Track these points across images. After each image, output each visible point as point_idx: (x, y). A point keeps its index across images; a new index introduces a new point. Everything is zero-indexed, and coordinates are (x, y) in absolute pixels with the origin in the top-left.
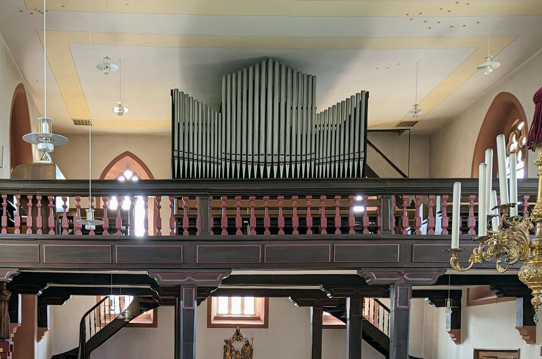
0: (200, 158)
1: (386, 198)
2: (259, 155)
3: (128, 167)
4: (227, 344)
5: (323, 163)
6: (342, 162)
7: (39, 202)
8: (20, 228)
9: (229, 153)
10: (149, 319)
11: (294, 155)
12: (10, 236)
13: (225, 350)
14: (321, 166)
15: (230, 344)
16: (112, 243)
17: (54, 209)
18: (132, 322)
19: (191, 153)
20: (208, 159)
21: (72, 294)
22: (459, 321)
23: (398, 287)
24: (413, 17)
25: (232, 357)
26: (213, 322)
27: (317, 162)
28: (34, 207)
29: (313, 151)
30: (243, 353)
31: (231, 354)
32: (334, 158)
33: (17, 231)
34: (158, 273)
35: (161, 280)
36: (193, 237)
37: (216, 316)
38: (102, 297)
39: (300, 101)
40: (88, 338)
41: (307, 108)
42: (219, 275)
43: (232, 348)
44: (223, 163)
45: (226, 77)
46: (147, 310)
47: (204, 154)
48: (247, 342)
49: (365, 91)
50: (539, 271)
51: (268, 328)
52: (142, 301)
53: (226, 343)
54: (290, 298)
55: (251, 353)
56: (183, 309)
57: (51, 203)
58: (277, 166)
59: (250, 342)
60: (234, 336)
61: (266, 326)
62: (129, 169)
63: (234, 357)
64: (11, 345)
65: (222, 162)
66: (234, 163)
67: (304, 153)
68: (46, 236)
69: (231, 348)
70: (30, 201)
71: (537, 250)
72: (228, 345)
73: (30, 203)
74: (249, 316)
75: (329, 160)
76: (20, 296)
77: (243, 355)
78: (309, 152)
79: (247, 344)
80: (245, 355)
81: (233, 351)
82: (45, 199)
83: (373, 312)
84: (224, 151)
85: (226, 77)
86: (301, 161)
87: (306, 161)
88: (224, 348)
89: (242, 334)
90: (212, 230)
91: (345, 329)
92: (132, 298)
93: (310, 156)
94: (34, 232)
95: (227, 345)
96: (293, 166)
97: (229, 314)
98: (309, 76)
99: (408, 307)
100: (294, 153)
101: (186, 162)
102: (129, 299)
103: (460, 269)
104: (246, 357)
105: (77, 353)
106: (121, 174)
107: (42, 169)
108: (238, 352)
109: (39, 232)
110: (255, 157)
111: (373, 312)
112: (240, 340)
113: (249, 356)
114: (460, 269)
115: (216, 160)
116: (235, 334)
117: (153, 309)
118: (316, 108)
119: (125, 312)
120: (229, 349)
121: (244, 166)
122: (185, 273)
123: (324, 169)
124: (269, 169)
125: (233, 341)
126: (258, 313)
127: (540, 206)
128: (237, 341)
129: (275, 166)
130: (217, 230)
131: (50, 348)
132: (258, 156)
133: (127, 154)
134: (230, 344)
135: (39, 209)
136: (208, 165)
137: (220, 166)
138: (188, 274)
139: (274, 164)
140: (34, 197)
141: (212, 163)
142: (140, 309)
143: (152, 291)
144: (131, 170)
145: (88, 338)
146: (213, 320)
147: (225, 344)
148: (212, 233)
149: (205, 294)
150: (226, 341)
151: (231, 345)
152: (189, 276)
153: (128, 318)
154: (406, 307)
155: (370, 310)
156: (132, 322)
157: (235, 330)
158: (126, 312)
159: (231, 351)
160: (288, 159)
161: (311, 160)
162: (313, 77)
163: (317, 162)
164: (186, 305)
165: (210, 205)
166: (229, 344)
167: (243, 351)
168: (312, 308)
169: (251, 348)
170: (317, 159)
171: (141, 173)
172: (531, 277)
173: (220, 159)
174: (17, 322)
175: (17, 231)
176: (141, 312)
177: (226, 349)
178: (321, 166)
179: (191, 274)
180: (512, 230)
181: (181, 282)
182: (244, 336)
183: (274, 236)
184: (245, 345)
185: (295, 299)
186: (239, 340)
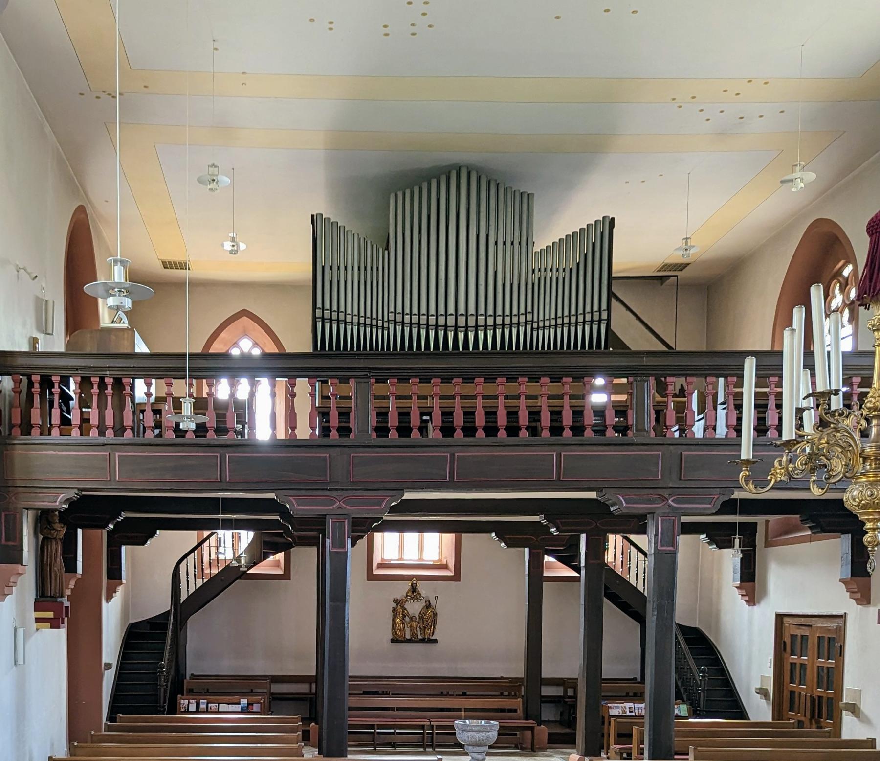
0: (355, 319)
1: (640, 381)
3: (245, 334)
4: (397, 605)
5: (544, 327)
7: (110, 387)
8: (80, 428)
9: (401, 312)
11: (499, 316)
12: (65, 439)
13: (394, 615)
14: (541, 332)
16: (222, 450)
17: (133, 398)
19: (342, 312)
20: (368, 321)
21: (160, 529)
23: (660, 518)
26: (376, 572)
27: (535, 325)
28: (102, 396)
29: (529, 309)
31: (403, 621)
32: (561, 319)
33: (75, 432)
36: (344, 441)
37: (380, 562)
38: (206, 534)
40: (184, 597)
41: (520, 243)
42: (385, 499)
44: (392, 327)
45: (396, 196)
49: (609, 217)
52: (267, 539)
53: (395, 604)
54: (493, 535)
55: (435, 619)
57: (128, 388)
58: (473, 332)
59: (433, 603)
60: (408, 592)
61: (456, 577)
62: (247, 337)
63: (407, 625)
64: (67, 608)
65: (390, 325)
67: (515, 312)
68: (120, 440)
69: (403, 612)
70: (95, 386)
72: (399, 607)
73: (95, 389)
74: (432, 563)
75: (553, 322)
76: (80, 531)
77: (422, 622)
78: (522, 311)
79: (428, 606)
80: (425, 622)
81: (407, 617)
82: (118, 384)
84: (392, 309)
85: (396, 196)
86: (511, 325)
87: (519, 324)
88: (392, 611)
89: (420, 590)
90: (374, 430)
92: (251, 534)
94: (102, 433)
100: (499, 311)
101: (335, 326)
102: (247, 537)
103: (754, 491)
105: (168, 619)
106: (236, 345)
107: (113, 337)
109: (110, 433)
110: (439, 318)
111: (621, 556)
112: (417, 599)
113: (430, 624)
114: (754, 491)
116: (409, 590)
117: (283, 552)
118: (534, 243)
121: (423, 333)
123: (545, 336)
125: (407, 601)
128: (412, 601)
129: (471, 331)
130: (382, 431)
131: (126, 610)
133: (245, 313)
135: (109, 399)
137: (386, 333)
138: (337, 497)
140: (102, 379)
142: (263, 552)
144: (250, 338)
145: (184, 597)
147: (394, 605)
148: (374, 435)
150: (396, 601)
151: (403, 607)
152: (340, 502)
154: (671, 548)
157: (410, 584)
159: (404, 617)
160: (490, 321)
161: (526, 323)
162: (528, 195)
163: (535, 325)
164: (334, 545)
166: (400, 606)
168: (527, 550)
169: (434, 612)
170: (535, 322)
172: (863, 502)
174: (76, 572)
175: (75, 432)
176: (265, 556)
177: (395, 612)
178: (541, 332)
179: (341, 498)
180: (834, 430)
182: (423, 593)
184: (425, 608)
185: (501, 537)
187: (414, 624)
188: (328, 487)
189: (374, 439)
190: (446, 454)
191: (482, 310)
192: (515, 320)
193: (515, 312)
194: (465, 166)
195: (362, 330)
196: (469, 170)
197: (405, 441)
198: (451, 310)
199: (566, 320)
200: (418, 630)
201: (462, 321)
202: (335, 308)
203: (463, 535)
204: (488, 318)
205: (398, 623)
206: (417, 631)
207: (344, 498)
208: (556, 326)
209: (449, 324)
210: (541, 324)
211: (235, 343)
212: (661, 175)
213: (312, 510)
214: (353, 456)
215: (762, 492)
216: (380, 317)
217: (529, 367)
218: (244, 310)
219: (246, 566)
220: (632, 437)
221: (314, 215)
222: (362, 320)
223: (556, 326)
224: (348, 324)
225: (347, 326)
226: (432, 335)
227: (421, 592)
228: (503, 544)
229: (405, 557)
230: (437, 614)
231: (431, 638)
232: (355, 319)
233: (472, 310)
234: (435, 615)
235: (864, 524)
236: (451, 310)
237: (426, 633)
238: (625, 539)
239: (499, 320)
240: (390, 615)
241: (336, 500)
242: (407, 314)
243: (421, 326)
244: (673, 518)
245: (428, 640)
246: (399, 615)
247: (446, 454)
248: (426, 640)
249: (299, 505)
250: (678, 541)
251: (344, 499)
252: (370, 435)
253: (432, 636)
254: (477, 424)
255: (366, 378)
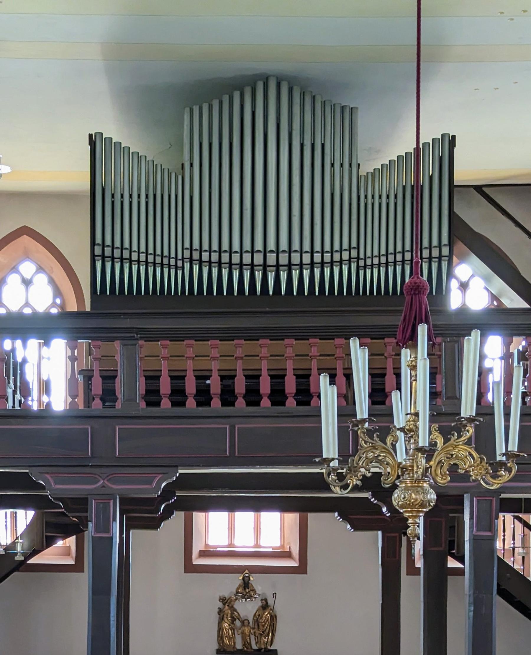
0: (143, 257)
1: (450, 342)
2: (253, 252)
3: (27, 256)
4: (224, 604)
5: (372, 265)
6: (407, 264)
9: (198, 248)
10: (69, 555)
11: (318, 252)
13: (220, 618)
14: (368, 272)
15: (230, 605)
18: (33, 561)
19: (126, 249)
20: (158, 260)
22: (397, 558)
23: (475, 499)
24: (513, 16)
25: (234, 631)
26: (197, 561)
27: (362, 263)
29: (354, 244)
30: (256, 624)
31: (233, 625)
32: (393, 256)
34: (48, 473)
35: (53, 486)
36: (109, 412)
37: (203, 549)
39: (329, 153)
41: (342, 165)
42: (157, 476)
43: (236, 613)
46: (64, 538)
47: (151, 251)
48: (264, 601)
49: (449, 134)
50: (407, 496)
51: (306, 573)
52: (53, 520)
53: (221, 604)
54: (336, 514)
55: (273, 624)
56: (92, 537)
58: (286, 272)
59: (270, 602)
60: (238, 589)
62: (29, 260)
63: (238, 632)
65: (185, 264)
66: (207, 267)
67: (337, 247)
69: (232, 613)
71: (410, 471)
72: (227, 607)
74: (271, 550)
75: (383, 260)
77: (256, 627)
78: (345, 246)
79: (265, 606)
80: (261, 627)
81: (237, 620)
83: (512, 542)
84: (187, 245)
86: (332, 263)
87: (341, 262)
88: (218, 613)
89: (254, 586)
90: (143, 398)
91: (463, 577)
92: (31, 514)
93: (348, 252)
95: (224, 607)
96: (317, 272)
97: (231, 545)
98: (344, 108)
99: (492, 533)
100: (318, 247)
101: (118, 266)
103: (340, 492)
104: (263, 632)
106: (14, 270)
108: (246, 621)
110: (245, 255)
111: (512, 542)
112: (250, 597)
113: (268, 630)
114: (340, 492)
115: (173, 262)
116: (240, 586)
117: (75, 536)
118: (359, 165)
119: (16, 541)
120: (227, 615)
122: (95, 474)
124: (271, 277)
125: (236, 599)
126: (289, 543)
127: (413, 418)
128: (244, 600)
129: (284, 271)
132: (250, 255)
133: (25, 231)
134: (230, 605)
136: (158, 270)
137: (180, 273)
138: (101, 475)
139: (281, 268)
141: (165, 266)
142: (46, 536)
143: (54, 502)
146: (197, 558)
147: (220, 605)
148: (143, 404)
149: (153, 508)
150: (223, 600)
151: (232, 607)
152: (104, 480)
153: (22, 553)
154: (489, 534)
155: (505, 537)
156: (33, 561)
157: (241, 578)
158: (18, 542)
159: (233, 620)
160: (306, 259)
161: (350, 260)
163: (362, 263)
164: (97, 530)
165: (140, 356)
166: (228, 606)
167: (256, 621)
168: (380, 533)
169: (272, 614)
170: (362, 259)
171: (51, 267)
172: (400, 503)
173: (180, 260)
176: (50, 542)
177: (222, 615)
178: (368, 272)
179: (105, 475)
180: (372, 448)
181: (88, 490)
182: (259, 589)
183: (252, 409)
184: (261, 609)
186: (248, 598)
187: (247, 630)
188: (90, 463)
189: (142, 409)
190: (225, 426)
191: (296, 246)
192: (337, 257)
193: (337, 247)
194: (273, 76)
195: (151, 270)
196: (279, 81)
197: (179, 411)
198: (259, 246)
199: (399, 257)
200: (252, 637)
201: (271, 259)
202: (118, 244)
203: (310, 515)
204: (304, 255)
205: (226, 629)
206: (250, 639)
207: (108, 476)
208: (387, 263)
209: (256, 263)
210: (369, 262)
211: (14, 268)
212: (516, 83)
213: (73, 490)
214: (118, 428)
215: (344, 493)
216: (173, 255)
217: (314, 327)
218: (25, 227)
219: (23, 554)
220: (441, 406)
221: (92, 134)
222: (151, 259)
223: (387, 263)
224: (133, 263)
225: (133, 266)
226: (236, 276)
227: (255, 588)
228: (349, 526)
229: (236, 542)
230: (276, 617)
231: (269, 647)
232: (143, 257)
233: (284, 245)
234: (274, 617)
235: (407, 520)
236: (259, 246)
237: (262, 641)
238: (517, 519)
239: (317, 258)
240: (215, 618)
241: (99, 478)
242: (206, 251)
243: (223, 265)
244: (491, 498)
245: (265, 650)
246: (227, 617)
247: (225, 426)
248: (263, 650)
249: (56, 484)
250: (496, 524)
251: (111, 476)
252: (138, 403)
253: (270, 647)
254: (262, 392)
255: (134, 340)
